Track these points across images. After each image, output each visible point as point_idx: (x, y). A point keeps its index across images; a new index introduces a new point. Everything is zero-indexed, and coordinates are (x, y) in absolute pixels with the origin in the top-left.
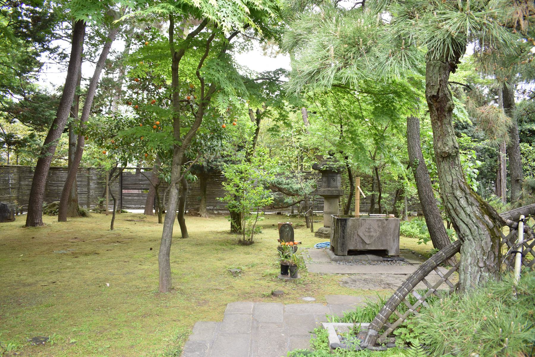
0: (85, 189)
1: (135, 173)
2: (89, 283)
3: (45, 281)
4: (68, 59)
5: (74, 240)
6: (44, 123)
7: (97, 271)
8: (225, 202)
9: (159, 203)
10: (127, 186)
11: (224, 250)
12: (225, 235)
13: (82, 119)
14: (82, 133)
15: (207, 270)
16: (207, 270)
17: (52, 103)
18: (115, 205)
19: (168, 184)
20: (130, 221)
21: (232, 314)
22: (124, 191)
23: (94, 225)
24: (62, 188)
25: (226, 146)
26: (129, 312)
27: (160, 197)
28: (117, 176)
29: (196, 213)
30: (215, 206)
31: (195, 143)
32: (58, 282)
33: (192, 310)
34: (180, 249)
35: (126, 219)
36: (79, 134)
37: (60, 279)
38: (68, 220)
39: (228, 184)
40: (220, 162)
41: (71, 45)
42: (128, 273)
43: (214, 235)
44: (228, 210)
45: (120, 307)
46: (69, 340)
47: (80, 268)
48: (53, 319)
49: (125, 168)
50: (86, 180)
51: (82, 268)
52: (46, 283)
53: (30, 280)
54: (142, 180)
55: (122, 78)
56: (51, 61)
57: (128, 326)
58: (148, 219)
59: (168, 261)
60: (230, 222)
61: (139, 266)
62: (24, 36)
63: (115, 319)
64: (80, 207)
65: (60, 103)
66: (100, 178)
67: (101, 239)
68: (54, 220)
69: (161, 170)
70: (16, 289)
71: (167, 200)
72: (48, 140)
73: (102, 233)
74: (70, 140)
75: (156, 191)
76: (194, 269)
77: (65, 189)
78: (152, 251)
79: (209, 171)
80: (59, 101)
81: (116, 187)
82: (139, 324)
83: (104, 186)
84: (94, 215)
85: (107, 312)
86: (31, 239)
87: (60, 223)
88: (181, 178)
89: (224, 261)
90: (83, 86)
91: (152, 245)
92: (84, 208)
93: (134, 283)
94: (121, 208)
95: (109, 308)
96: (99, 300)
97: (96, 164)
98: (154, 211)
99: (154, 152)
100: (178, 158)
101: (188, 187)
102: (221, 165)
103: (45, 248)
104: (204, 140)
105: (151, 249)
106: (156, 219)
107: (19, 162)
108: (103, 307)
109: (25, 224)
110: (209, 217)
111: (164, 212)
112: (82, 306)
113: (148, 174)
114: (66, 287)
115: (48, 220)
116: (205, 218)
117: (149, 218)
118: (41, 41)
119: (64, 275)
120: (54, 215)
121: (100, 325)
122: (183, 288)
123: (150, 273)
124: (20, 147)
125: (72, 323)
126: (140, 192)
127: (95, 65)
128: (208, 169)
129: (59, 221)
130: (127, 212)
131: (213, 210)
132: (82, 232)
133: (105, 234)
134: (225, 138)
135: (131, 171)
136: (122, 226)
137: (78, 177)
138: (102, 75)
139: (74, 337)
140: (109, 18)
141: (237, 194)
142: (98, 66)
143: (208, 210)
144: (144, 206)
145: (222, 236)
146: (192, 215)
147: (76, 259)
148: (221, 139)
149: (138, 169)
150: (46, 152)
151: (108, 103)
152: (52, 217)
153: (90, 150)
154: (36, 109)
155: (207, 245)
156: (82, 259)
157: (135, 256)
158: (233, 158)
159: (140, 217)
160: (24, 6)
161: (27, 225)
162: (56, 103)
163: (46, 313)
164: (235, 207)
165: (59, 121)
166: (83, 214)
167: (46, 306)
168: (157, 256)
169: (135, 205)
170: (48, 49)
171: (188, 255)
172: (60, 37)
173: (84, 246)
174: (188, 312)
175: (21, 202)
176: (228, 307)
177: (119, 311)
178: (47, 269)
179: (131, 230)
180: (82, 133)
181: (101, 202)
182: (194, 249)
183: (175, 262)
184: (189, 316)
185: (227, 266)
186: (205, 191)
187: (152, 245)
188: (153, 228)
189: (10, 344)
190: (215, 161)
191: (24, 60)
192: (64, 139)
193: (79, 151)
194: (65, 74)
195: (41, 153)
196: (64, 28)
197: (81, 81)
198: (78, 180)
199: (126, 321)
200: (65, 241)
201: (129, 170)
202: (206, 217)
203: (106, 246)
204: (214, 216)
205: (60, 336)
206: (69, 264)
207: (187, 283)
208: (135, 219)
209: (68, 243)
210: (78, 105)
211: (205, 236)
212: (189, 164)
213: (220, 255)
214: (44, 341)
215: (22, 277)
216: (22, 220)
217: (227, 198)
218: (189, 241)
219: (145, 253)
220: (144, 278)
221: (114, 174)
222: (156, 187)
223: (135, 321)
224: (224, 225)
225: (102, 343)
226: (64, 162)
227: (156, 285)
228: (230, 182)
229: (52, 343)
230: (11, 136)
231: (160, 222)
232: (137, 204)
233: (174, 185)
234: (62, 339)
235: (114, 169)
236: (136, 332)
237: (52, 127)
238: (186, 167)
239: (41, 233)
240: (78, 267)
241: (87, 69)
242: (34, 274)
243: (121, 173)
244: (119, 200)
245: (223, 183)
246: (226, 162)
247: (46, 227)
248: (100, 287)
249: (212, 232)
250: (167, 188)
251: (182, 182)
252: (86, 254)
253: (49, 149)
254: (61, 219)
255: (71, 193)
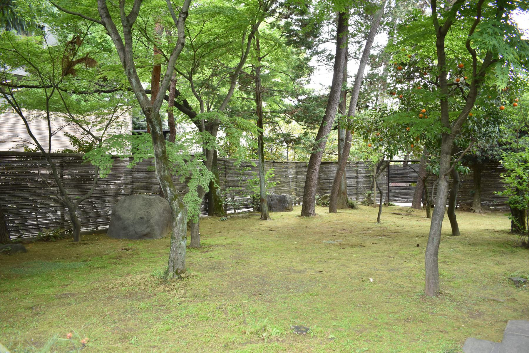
0: (354, 183)
1: (402, 166)
2: (353, 276)
3: (313, 269)
4: (334, 60)
5: (342, 231)
6: (315, 120)
7: (362, 264)
8: (504, 197)
9: (427, 197)
10: (394, 179)
11: (503, 252)
12: (504, 235)
13: (349, 115)
14: (349, 127)
15: (482, 275)
16: (482, 275)
17: (322, 101)
18: (381, 198)
19: (436, 177)
20: (397, 214)
21: (513, 335)
22: (392, 184)
23: (361, 217)
24: (333, 181)
25: (505, 132)
26: (391, 313)
27: (429, 190)
28: (383, 169)
29: (469, 208)
30: (492, 201)
31: (468, 130)
32: (324, 272)
33: (463, 322)
34: (451, 248)
35: (393, 212)
36: (347, 128)
37: (326, 268)
38: (338, 211)
39: (507, 176)
40: (496, 151)
41: (336, 46)
42: (393, 270)
43: (490, 235)
44: (506, 205)
45: (382, 306)
46: (328, 334)
47: (345, 260)
48: (316, 309)
49: (391, 161)
50: (355, 173)
51: (348, 260)
52: (313, 272)
53: (300, 268)
54: (408, 173)
55: (387, 70)
56: (320, 64)
57: (389, 329)
58: (415, 213)
59: (435, 262)
60: (511, 220)
61: (405, 263)
62: (296, 45)
63: (376, 319)
64: (349, 199)
65: (328, 101)
66: (368, 172)
67: (367, 232)
68: (326, 211)
69: (429, 162)
70: (287, 275)
71: (435, 193)
72: (320, 135)
73: (369, 225)
74: (339, 136)
75: (424, 184)
76: (466, 272)
77: (335, 182)
78: (419, 248)
79: (483, 161)
80: (327, 99)
81: (383, 180)
82: (399, 328)
83: (372, 179)
84: (361, 207)
85: (368, 309)
86: (305, 228)
87: (331, 214)
88: (451, 169)
89: (503, 267)
90: (349, 84)
91: (419, 241)
92: (353, 201)
93: (398, 281)
94: (389, 201)
95: (370, 306)
96: (361, 295)
97: (364, 157)
98: (422, 205)
99: (420, 142)
100: (446, 147)
101: (459, 180)
102: (498, 155)
103: (316, 237)
104: (478, 126)
105: (418, 245)
106: (424, 213)
107: (296, 158)
108: (364, 303)
109: (300, 214)
110: (484, 213)
111: (432, 206)
112: (344, 299)
113: (416, 166)
114: (331, 278)
115: (321, 211)
116: (479, 214)
117: (417, 212)
118: (309, 47)
119: (331, 265)
120: (326, 206)
121: (360, 323)
122: (452, 293)
123: (415, 272)
124: (296, 144)
125: (333, 316)
126: (408, 185)
127: (359, 62)
128: (482, 160)
129: (330, 212)
130: (394, 205)
131: (488, 205)
132: (350, 223)
133: (371, 227)
134: (503, 122)
135: (399, 163)
136: (389, 219)
137: (347, 171)
138: (367, 70)
139: (333, 332)
140: (370, 10)
141: (519, 187)
142: (362, 62)
143: (482, 205)
144: (412, 200)
145: (500, 236)
146: (464, 211)
147: (343, 250)
148: (499, 123)
149: (406, 162)
150: (317, 148)
151: (374, 98)
152: (324, 208)
153: (357, 145)
154: (307, 109)
155: (482, 245)
156: (348, 250)
157: (400, 252)
158: (514, 145)
159: (407, 211)
160: (293, 16)
161: (302, 215)
162: (325, 101)
163: (310, 302)
164: (518, 202)
165: (328, 118)
166: (352, 207)
167: (311, 295)
168: (424, 254)
169: (402, 198)
170: (317, 53)
171: (459, 256)
172: (327, 41)
173: (351, 238)
174: (457, 324)
175: (298, 194)
176: (508, 325)
177: (381, 310)
178: (316, 257)
179: (398, 224)
180: (349, 127)
181: (369, 195)
182: (467, 249)
183: (444, 262)
184: (458, 328)
185: (508, 272)
186: (479, 184)
187: (419, 241)
188: (420, 223)
189: (275, 329)
190: (490, 150)
191: (297, 66)
192: (333, 135)
193: (347, 146)
194: (331, 74)
195: (313, 149)
196: (328, 29)
197: (348, 79)
198: (346, 172)
199: (387, 323)
200: (333, 232)
201: (396, 163)
202: (480, 213)
203: (372, 238)
204: (490, 212)
205: (320, 329)
206: (336, 255)
207: (458, 288)
208: (402, 212)
209: (337, 234)
210: (345, 102)
211: (480, 235)
212: (459, 154)
213: (498, 259)
214: (305, 331)
215: (293, 263)
216: (298, 210)
217: (508, 192)
218: (460, 240)
219: (411, 249)
220: (409, 277)
221: (381, 168)
222: (424, 180)
223: (397, 325)
224: (503, 223)
225: (360, 343)
226: (334, 158)
227: (422, 286)
228: (510, 173)
229: (312, 335)
230: (288, 135)
231: (428, 216)
232: (405, 198)
233: (443, 177)
234: (321, 332)
235: (381, 162)
236: (396, 337)
237: (322, 124)
238: (456, 158)
239: (313, 223)
240: (344, 258)
241: (352, 67)
242: (304, 261)
243: (388, 165)
244: (386, 193)
245: (502, 175)
246: (505, 150)
247: (318, 218)
248: (363, 281)
249: (488, 231)
250: (436, 180)
251: (453, 174)
252: (352, 246)
253: (319, 145)
254: (332, 210)
255: (340, 186)
